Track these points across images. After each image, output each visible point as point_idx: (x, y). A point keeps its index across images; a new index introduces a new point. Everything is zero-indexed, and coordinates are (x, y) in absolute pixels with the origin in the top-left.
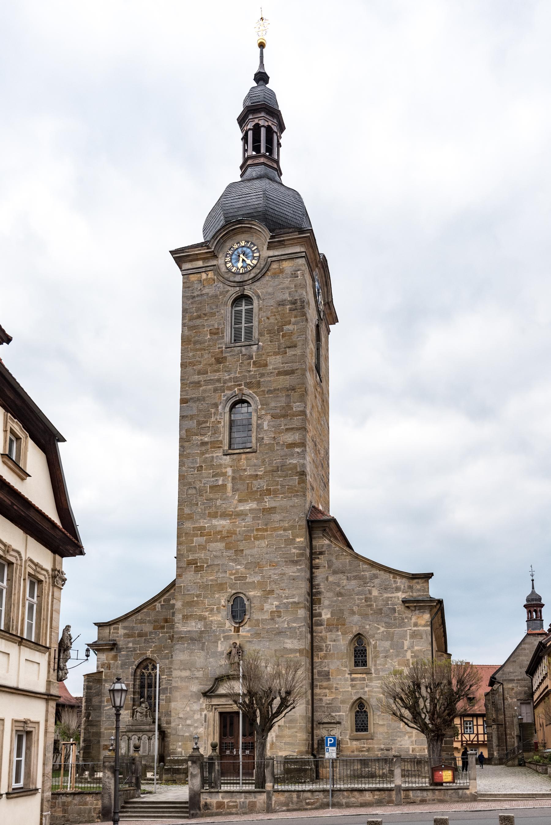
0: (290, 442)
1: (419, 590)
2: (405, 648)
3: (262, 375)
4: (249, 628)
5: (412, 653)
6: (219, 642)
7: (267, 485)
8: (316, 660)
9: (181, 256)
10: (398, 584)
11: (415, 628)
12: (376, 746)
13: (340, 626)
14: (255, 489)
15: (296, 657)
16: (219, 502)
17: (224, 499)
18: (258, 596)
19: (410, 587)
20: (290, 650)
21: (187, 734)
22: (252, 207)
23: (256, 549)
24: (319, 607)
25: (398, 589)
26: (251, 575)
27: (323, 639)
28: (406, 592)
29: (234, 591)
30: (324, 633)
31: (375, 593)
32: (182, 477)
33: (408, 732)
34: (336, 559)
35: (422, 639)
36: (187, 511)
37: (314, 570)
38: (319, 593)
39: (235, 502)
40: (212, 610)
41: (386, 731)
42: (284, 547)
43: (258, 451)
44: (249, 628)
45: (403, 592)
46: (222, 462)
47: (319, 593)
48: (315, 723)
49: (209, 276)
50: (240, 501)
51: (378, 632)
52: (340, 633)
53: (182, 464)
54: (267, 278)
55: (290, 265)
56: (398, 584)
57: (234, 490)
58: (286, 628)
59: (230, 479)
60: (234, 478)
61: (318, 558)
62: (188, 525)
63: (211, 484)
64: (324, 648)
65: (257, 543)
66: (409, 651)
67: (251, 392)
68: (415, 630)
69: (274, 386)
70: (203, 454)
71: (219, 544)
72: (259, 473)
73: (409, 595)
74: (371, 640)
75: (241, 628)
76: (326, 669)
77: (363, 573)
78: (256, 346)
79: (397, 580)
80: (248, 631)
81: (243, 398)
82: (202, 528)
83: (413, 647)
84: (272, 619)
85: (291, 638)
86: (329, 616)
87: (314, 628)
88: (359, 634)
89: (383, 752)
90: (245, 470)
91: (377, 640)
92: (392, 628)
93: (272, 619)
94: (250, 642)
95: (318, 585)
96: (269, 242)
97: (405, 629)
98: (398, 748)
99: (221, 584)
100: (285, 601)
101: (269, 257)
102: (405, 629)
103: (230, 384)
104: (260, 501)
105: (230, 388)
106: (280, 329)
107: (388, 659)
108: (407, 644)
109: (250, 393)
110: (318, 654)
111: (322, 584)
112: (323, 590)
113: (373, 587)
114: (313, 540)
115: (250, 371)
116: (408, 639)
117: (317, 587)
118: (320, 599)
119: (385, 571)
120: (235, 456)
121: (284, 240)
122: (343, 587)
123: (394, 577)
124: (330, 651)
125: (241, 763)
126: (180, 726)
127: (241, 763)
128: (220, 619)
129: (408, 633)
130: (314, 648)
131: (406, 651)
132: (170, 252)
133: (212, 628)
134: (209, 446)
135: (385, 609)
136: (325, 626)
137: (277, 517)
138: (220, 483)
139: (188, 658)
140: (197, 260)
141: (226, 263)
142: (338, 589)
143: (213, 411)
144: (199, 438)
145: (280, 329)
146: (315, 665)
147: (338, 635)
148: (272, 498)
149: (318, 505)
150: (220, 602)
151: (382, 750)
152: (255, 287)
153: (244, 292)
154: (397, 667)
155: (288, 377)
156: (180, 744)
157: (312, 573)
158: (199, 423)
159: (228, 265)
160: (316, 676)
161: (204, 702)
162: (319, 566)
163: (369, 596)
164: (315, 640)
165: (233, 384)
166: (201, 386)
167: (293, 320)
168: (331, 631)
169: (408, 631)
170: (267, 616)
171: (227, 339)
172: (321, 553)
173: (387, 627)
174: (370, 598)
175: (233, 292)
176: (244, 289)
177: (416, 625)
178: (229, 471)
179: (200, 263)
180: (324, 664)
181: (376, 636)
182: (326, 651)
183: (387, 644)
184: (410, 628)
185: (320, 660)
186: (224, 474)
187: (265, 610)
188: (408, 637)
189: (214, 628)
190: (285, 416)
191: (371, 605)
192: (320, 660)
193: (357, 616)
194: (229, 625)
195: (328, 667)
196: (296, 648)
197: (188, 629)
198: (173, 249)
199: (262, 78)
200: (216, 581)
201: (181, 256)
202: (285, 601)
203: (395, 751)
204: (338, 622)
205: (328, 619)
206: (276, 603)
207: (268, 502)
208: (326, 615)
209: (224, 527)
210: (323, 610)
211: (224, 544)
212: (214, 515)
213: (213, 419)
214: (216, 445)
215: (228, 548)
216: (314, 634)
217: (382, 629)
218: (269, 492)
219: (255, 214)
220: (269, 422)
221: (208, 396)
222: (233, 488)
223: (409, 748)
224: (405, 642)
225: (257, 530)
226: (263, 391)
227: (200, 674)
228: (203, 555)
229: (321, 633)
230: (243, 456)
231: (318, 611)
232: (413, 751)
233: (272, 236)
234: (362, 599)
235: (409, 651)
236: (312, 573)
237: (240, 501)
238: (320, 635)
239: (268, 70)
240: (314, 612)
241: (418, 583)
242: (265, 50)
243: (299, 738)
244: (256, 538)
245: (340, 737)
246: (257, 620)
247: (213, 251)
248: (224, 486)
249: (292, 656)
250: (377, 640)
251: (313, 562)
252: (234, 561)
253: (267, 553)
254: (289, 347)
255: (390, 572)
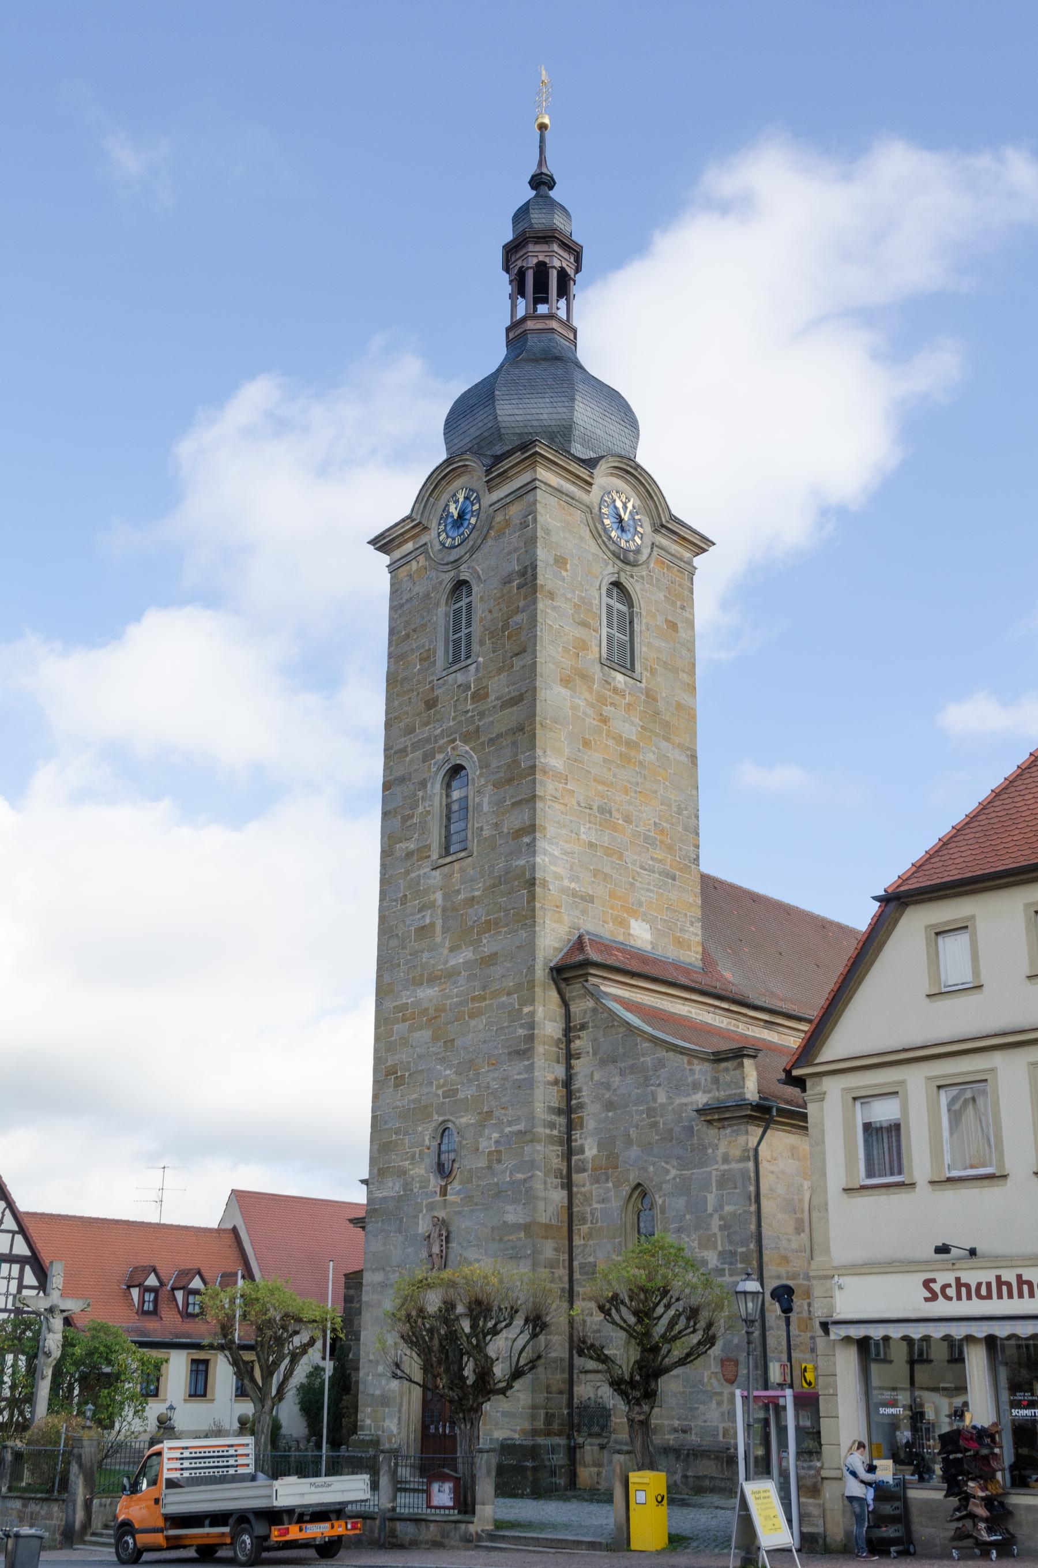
0: (517, 827)
1: (729, 1085)
2: (710, 1210)
3: (482, 715)
4: (460, 1187)
5: (720, 1220)
6: (421, 1216)
7: (488, 914)
8: (577, 1241)
9: (383, 543)
10: (696, 1076)
11: (725, 1167)
12: (666, 1423)
13: (610, 1171)
14: (470, 923)
15: (519, 1239)
16: (425, 957)
17: (432, 950)
18: (472, 1125)
19: (716, 1080)
20: (513, 1225)
21: (378, 1392)
22: (480, 424)
23: (470, 1036)
24: (581, 1134)
25: (696, 1086)
26: (463, 1084)
27: (587, 1199)
28: (709, 1092)
29: (441, 1119)
30: (588, 1187)
31: (662, 1098)
32: (382, 919)
33: (716, 1393)
34: (604, 1035)
35: (736, 1188)
36: (387, 979)
37: (573, 1062)
38: (581, 1106)
39: (446, 952)
40: (413, 1157)
41: (682, 1390)
42: (507, 1027)
43: (475, 854)
44: (460, 1187)
45: (705, 1092)
46: (431, 882)
47: (581, 1106)
48: (576, 1371)
49: (420, 564)
50: (452, 950)
51: (668, 1178)
52: (610, 1185)
53: (382, 899)
54: (490, 542)
55: (520, 508)
56: (696, 1076)
57: (445, 930)
58: (508, 1182)
59: (439, 912)
60: (444, 910)
61: (579, 1038)
62: (389, 1004)
63: (417, 925)
64: (589, 1217)
65: (473, 1023)
66: (716, 1217)
67: (467, 748)
68: (725, 1171)
69: (498, 729)
70: (407, 872)
71: (424, 1032)
72: (476, 893)
73: (713, 1098)
74: (657, 1196)
75: (449, 1187)
76: (591, 1259)
77: (642, 1059)
78: (474, 665)
79: (695, 1067)
80: (458, 1193)
81: (458, 762)
82: (404, 1007)
83: (722, 1207)
84: (490, 1167)
85: (514, 1201)
86: (594, 1152)
87: (574, 1176)
88: (639, 1185)
89: (676, 1435)
90: (458, 891)
91: (665, 1195)
92: (688, 1170)
93: (490, 1167)
94: (459, 1213)
95: (580, 1090)
96: (487, 482)
97: (709, 1169)
98: (702, 1427)
99: (426, 1107)
100: (507, 1130)
101: (491, 506)
102: (709, 1169)
103: (441, 742)
104: (477, 944)
105: (441, 749)
106: (506, 626)
107: (683, 1236)
108: (711, 1199)
109: (467, 752)
110: (579, 1230)
111: (585, 1088)
112: (587, 1100)
113: (659, 1085)
114: (571, 1003)
115: (467, 712)
116: (714, 1190)
117: (578, 1095)
118: (582, 1118)
119: (675, 1051)
120: (446, 869)
121: (505, 472)
122: (615, 1090)
123: (690, 1063)
124: (597, 1222)
125: (324, 1458)
126: (370, 1377)
127: (324, 1458)
128: (422, 1172)
129: (714, 1179)
130: (575, 1218)
131: (711, 1215)
132: (369, 543)
133: (412, 1190)
134: (415, 857)
135: (677, 1129)
136: (590, 1172)
137: (498, 970)
138: (428, 921)
139: (382, 1249)
140: (406, 541)
141: (439, 535)
142: (607, 1096)
143: (420, 794)
144: (403, 845)
145: (506, 626)
146: (576, 1251)
147: (608, 1190)
148: (491, 936)
149: (623, 923)
150: (424, 1140)
151: (676, 1430)
152: (473, 564)
153: (459, 576)
154: (697, 1250)
155: (515, 708)
156: (369, 1409)
157: (569, 1067)
158: (405, 819)
159: (441, 538)
160: (577, 1276)
161: (695, 1301)
162: (579, 1054)
163: (652, 1105)
164: (576, 1201)
165: (446, 740)
166: (407, 755)
167: (521, 604)
168: (598, 1182)
169: (714, 1173)
170: (482, 1163)
171: (440, 663)
172: (583, 1027)
173: (682, 1167)
174: (654, 1109)
175: (447, 578)
176: (460, 572)
177: (726, 1159)
178: (438, 896)
179: (409, 546)
180: (587, 1250)
181: (664, 1186)
182: (592, 1223)
183: (681, 1202)
184: (716, 1167)
185: (582, 1242)
186: (432, 905)
187: (481, 1150)
188: (714, 1185)
189: (415, 1190)
190: (509, 781)
191: (656, 1123)
192: (582, 1242)
193: (635, 1148)
194: (435, 1183)
195: (595, 1257)
196: (521, 1221)
197: (385, 1194)
198: (372, 537)
199: (541, 182)
200: (420, 1101)
201: (383, 543)
202: (507, 1130)
203: (696, 1434)
204: (609, 1165)
205: (594, 1158)
206: (495, 1136)
207: (489, 945)
208: (591, 1151)
209: (430, 1001)
210: (586, 1139)
211: (430, 1032)
212: (417, 983)
213: (420, 809)
214: (422, 853)
215: (435, 1038)
216: (575, 1189)
217: (673, 1172)
218: (489, 926)
219: (486, 434)
220: (490, 797)
221: (416, 770)
222: (443, 927)
223: (717, 1427)
224: (709, 1195)
225: (473, 999)
226: (483, 743)
227: (394, 1277)
228: (404, 1056)
229: (584, 1186)
230: (457, 865)
231: (579, 1142)
232: (724, 1436)
233: (487, 471)
234: (642, 1112)
235: (716, 1217)
236: (569, 1067)
237: (452, 950)
238: (583, 1189)
239: (553, 167)
240: (573, 1144)
241: (727, 1069)
242: (547, 133)
243: (522, 1402)
244: (472, 1016)
245: (612, 1402)
246: (470, 1170)
247: (420, 523)
248: (432, 925)
249: (513, 1237)
250: (665, 1195)
251: (572, 1045)
252: (442, 1060)
253: (484, 1042)
254: (517, 655)
255: (682, 1053)
